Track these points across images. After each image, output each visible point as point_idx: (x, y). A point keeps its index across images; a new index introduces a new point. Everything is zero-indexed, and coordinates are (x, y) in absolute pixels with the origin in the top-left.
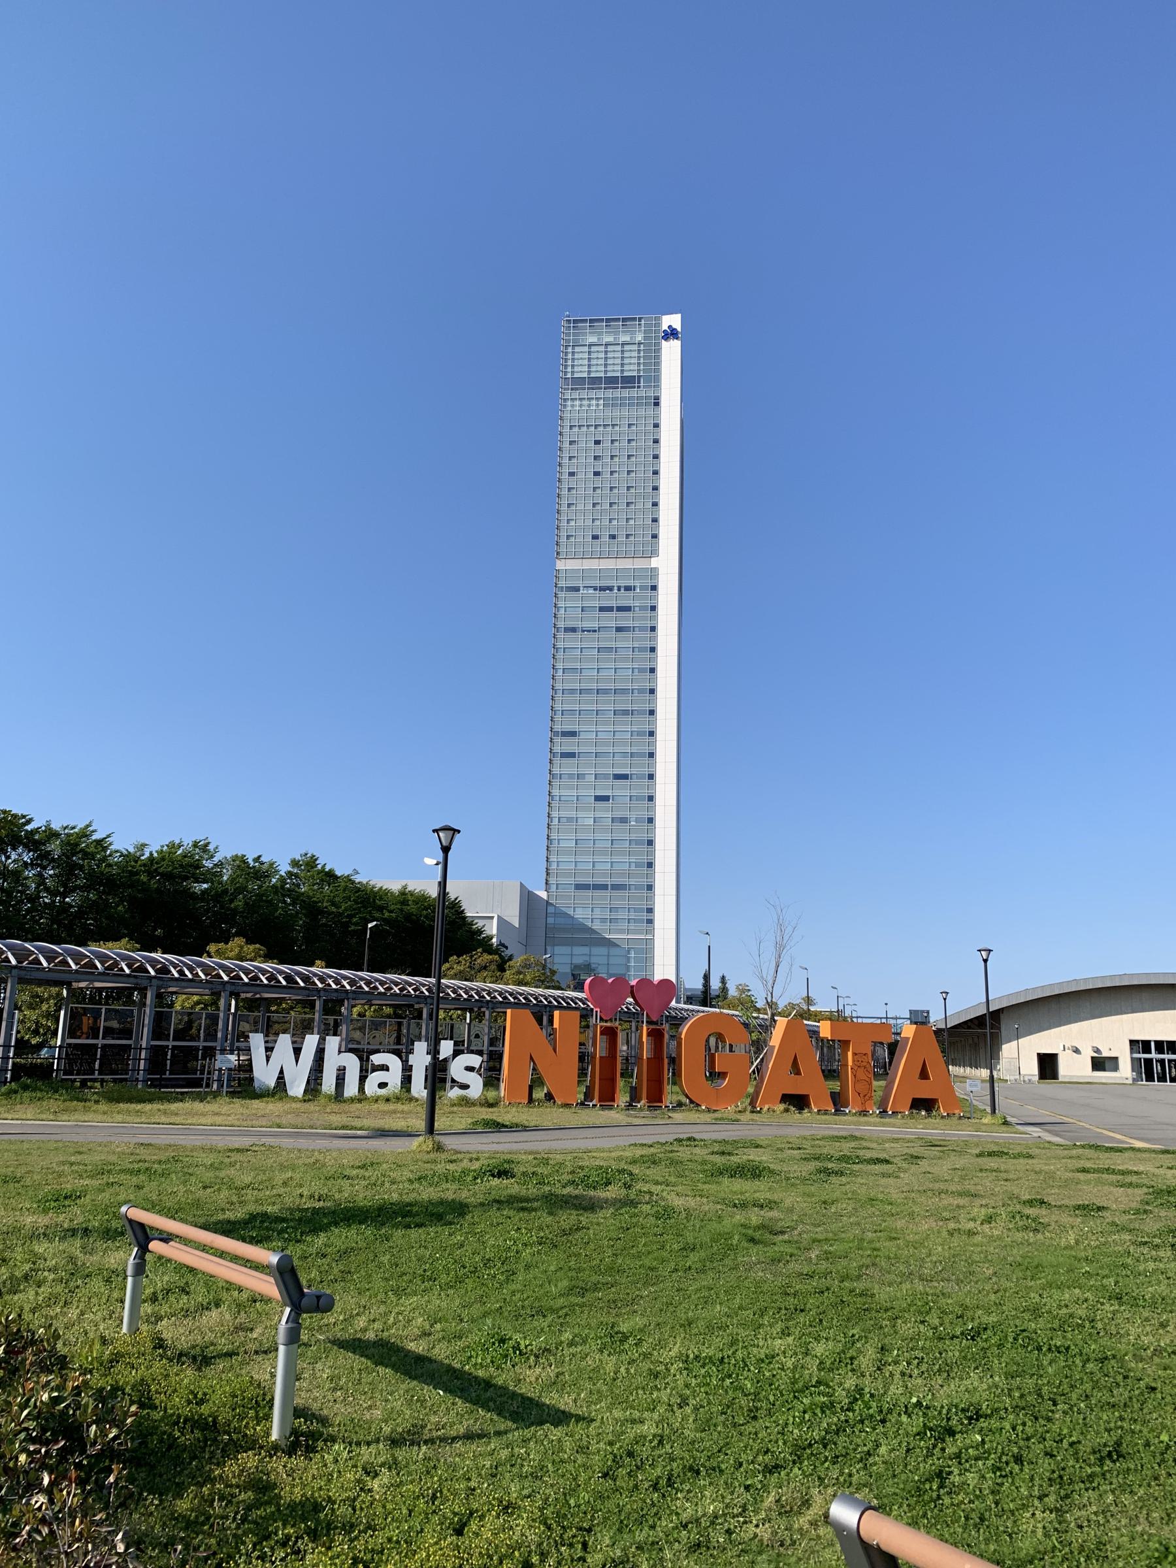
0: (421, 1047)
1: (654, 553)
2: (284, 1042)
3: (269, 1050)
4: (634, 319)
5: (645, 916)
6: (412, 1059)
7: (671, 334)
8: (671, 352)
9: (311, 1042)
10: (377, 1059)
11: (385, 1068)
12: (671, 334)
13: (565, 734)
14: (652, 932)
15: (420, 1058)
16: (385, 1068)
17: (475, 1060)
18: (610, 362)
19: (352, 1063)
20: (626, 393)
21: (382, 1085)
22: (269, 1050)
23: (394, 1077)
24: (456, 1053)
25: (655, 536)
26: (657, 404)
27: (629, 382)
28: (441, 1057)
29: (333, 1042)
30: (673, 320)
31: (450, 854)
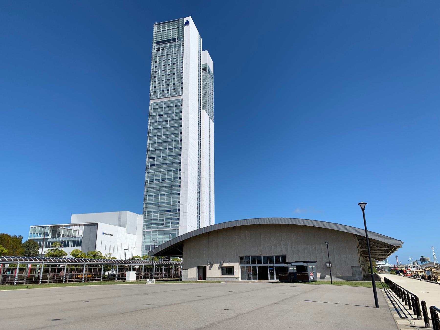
13: (152, 158)
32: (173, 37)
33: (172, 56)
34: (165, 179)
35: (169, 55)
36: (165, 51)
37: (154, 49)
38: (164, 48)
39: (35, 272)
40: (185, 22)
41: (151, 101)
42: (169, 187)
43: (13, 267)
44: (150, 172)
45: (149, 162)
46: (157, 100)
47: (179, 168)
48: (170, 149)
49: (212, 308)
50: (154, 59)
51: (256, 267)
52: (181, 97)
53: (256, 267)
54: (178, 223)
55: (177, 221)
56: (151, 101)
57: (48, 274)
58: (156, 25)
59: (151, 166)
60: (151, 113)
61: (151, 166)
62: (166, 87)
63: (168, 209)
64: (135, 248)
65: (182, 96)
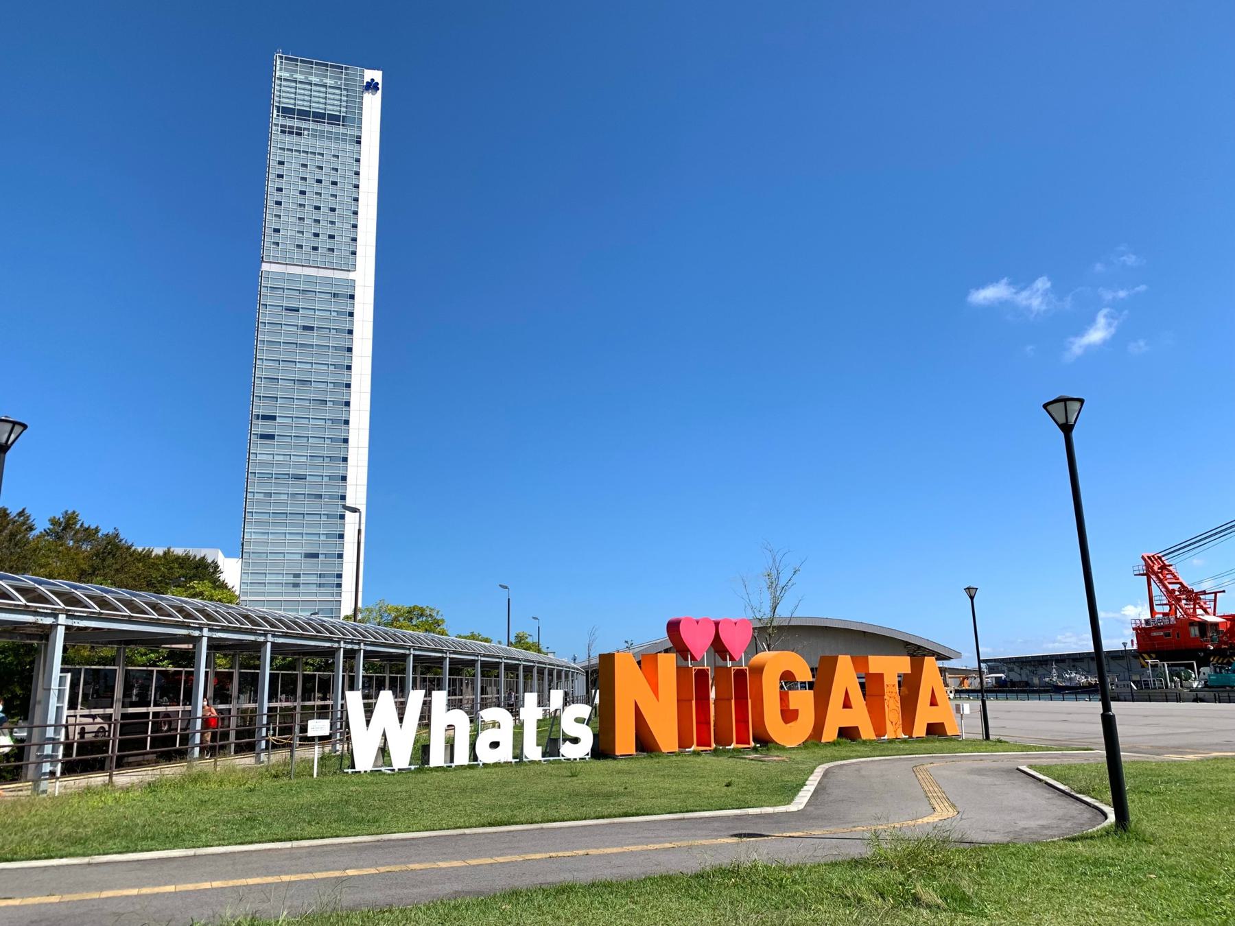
0: (531, 698)
1: (352, 267)
2: (386, 698)
3: (369, 710)
4: (341, 68)
5: (336, 581)
6: (524, 713)
7: (372, 86)
8: (372, 105)
9: (416, 698)
10: (488, 714)
11: (496, 725)
12: (372, 86)
13: (265, 418)
14: (340, 594)
15: (531, 711)
16: (496, 725)
17: (584, 710)
18: (322, 101)
19: (460, 719)
20: (334, 129)
21: (495, 745)
22: (369, 710)
23: (505, 735)
24: (566, 703)
25: (354, 253)
26: (359, 142)
27: (334, 119)
28: (552, 709)
29: (440, 698)
30: (376, 75)
31: (1075, 434)
32: (332, 110)
33: (327, 159)
34: (304, 477)
35: (319, 154)
36: (304, 142)
37: (277, 125)
38: (306, 132)
39: (332, 124)
40: (367, 82)
41: (264, 264)
42: (313, 496)
43: (1044, 872)
44: (262, 453)
45: (260, 427)
46: (281, 265)
47: (343, 454)
48: (319, 402)
49: (429, 782)
50: (275, 155)
51: (179, 711)
52: (351, 276)
53: (179, 711)
54: (339, 585)
55: (336, 581)
56: (264, 264)
57: (956, 688)
58: (281, 58)
59: (263, 436)
60: (267, 298)
61: (263, 436)
62: (308, 240)
63: (313, 550)
64: (500, 586)
65: (354, 273)
